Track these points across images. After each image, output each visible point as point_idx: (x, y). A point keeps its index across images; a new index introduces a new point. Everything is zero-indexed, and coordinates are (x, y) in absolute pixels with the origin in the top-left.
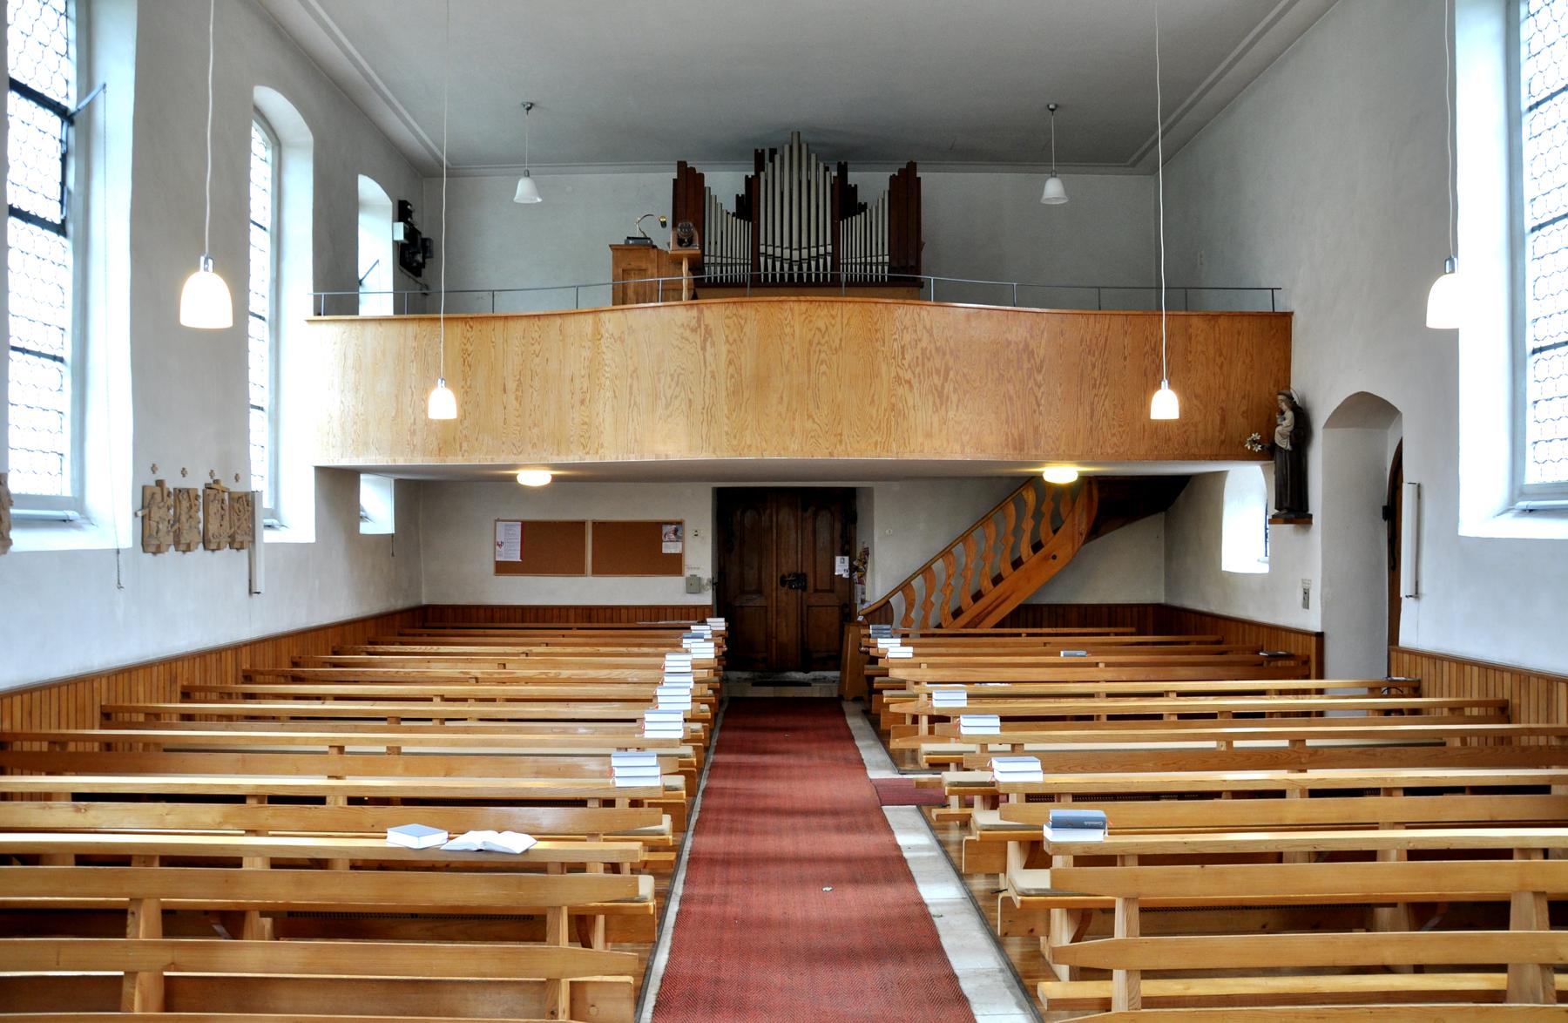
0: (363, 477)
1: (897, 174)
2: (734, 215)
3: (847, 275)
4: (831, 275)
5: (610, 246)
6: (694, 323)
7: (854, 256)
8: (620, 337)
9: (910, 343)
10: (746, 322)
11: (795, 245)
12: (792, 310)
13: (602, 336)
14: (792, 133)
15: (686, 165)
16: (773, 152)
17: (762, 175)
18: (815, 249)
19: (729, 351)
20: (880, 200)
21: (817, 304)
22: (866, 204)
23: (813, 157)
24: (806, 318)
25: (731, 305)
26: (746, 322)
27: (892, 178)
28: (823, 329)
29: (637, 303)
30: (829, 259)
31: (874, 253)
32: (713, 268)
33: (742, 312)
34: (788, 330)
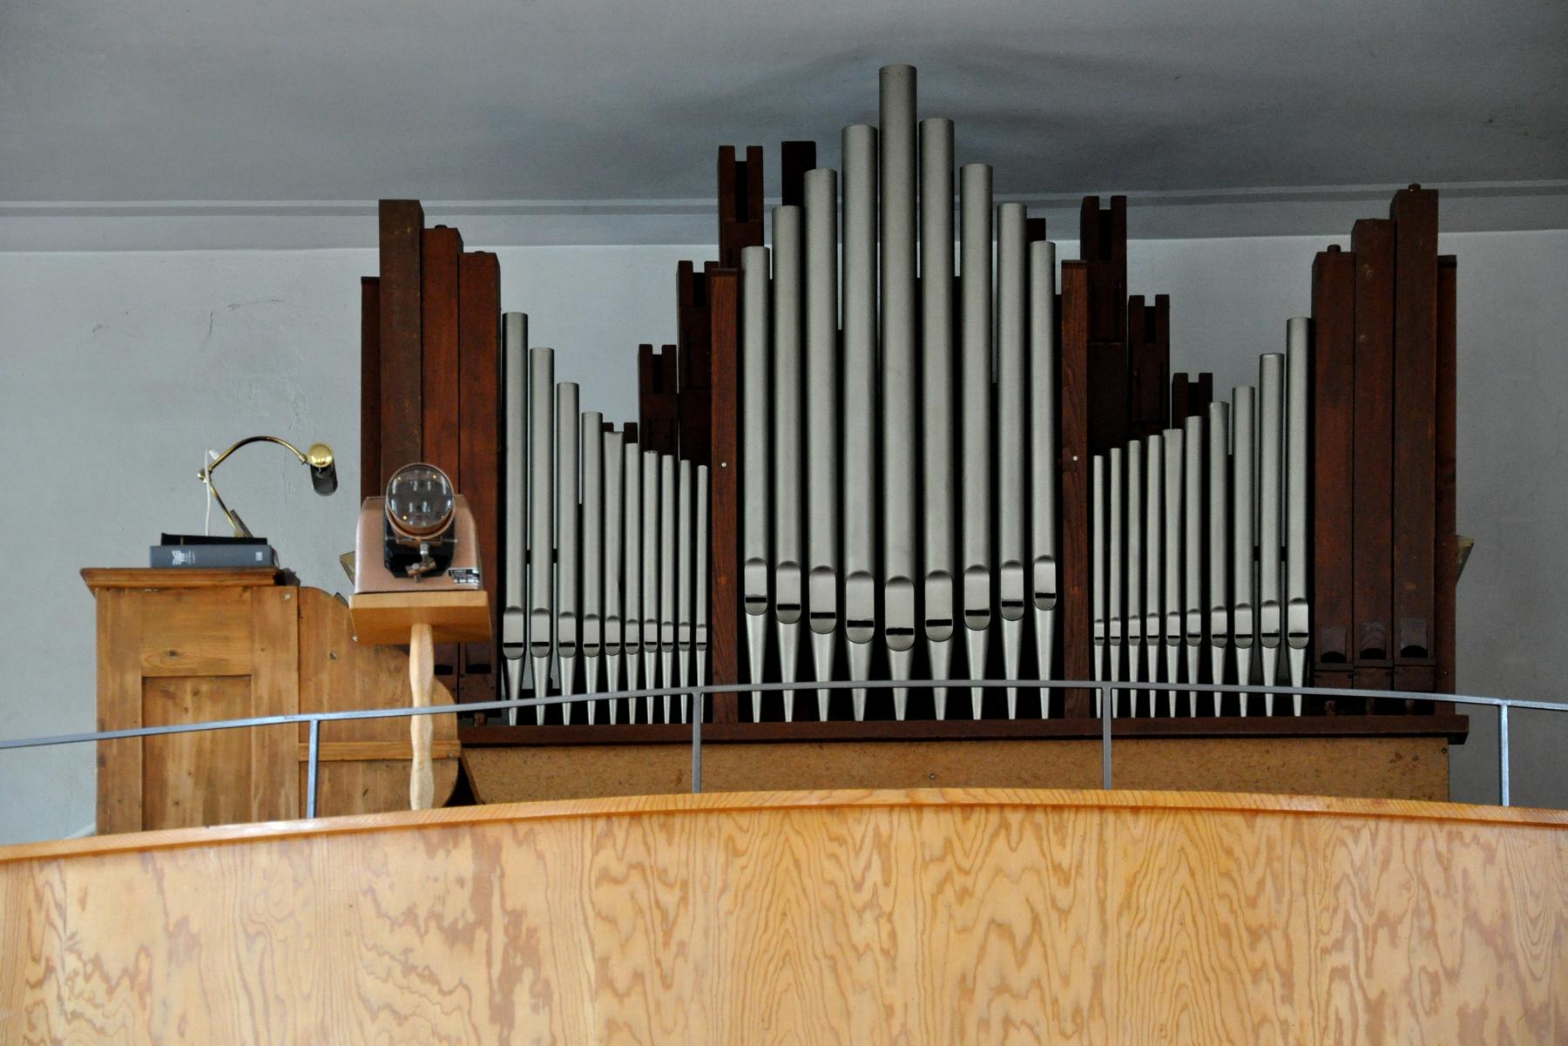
1: (1345, 243)
2: (629, 433)
3: (1124, 695)
4: (1053, 691)
5: (87, 573)
6: (459, 905)
7: (1153, 606)
8: (131, 974)
9: (1407, 984)
10: (684, 899)
11: (898, 563)
12: (883, 846)
13: (50, 970)
14: (882, 73)
15: (420, 215)
16: (799, 157)
17: (753, 258)
18: (985, 579)
19: (611, 1025)
20: (1272, 363)
21: (994, 817)
22: (1206, 379)
23: (975, 177)
24: (948, 878)
25: (620, 829)
26: (684, 899)
27: (1326, 263)
28: (1021, 927)
29: (211, 819)
30: (1044, 621)
31: (1242, 594)
32: (540, 664)
33: (670, 853)
34: (866, 931)
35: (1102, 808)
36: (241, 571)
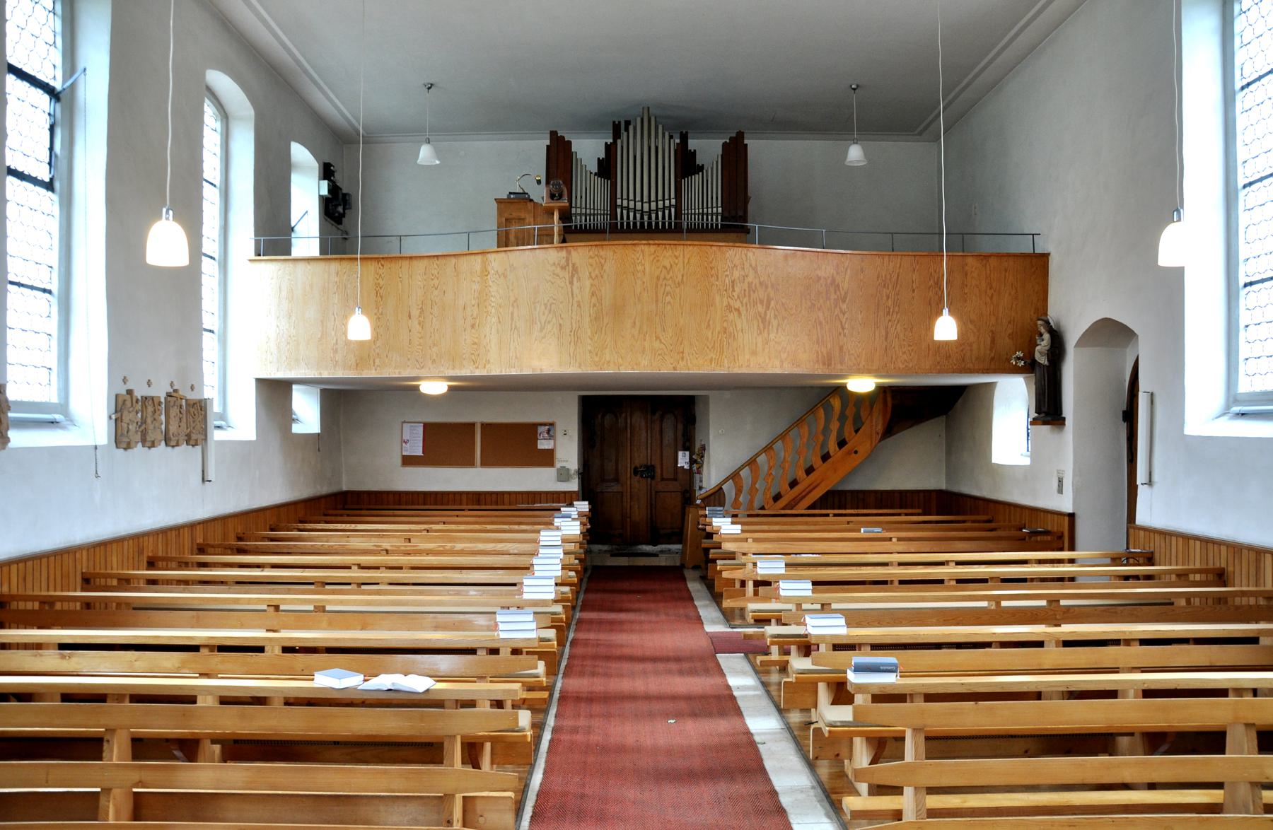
0: (294, 387)
1: (728, 141)
2: (596, 174)
3: (688, 223)
4: (675, 223)
5: (495, 199)
7: (693, 208)
8: (503, 274)
9: (739, 278)
10: (605, 261)
11: (645, 199)
12: (643, 251)
14: (643, 108)
15: (557, 134)
16: (628, 123)
17: (619, 142)
18: (662, 202)
19: (592, 285)
20: (715, 163)
21: (664, 246)
22: (703, 165)
23: (660, 127)
24: (655, 258)
25: (594, 248)
26: (605, 261)
27: (725, 145)
28: (668, 267)
29: (517, 246)
30: (673, 210)
31: (710, 206)
32: (578, 217)
33: (602, 253)
34: (639, 268)
35: (684, 245)
36: (523, 199)
